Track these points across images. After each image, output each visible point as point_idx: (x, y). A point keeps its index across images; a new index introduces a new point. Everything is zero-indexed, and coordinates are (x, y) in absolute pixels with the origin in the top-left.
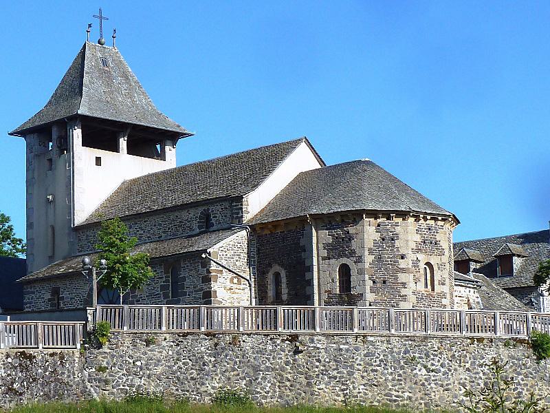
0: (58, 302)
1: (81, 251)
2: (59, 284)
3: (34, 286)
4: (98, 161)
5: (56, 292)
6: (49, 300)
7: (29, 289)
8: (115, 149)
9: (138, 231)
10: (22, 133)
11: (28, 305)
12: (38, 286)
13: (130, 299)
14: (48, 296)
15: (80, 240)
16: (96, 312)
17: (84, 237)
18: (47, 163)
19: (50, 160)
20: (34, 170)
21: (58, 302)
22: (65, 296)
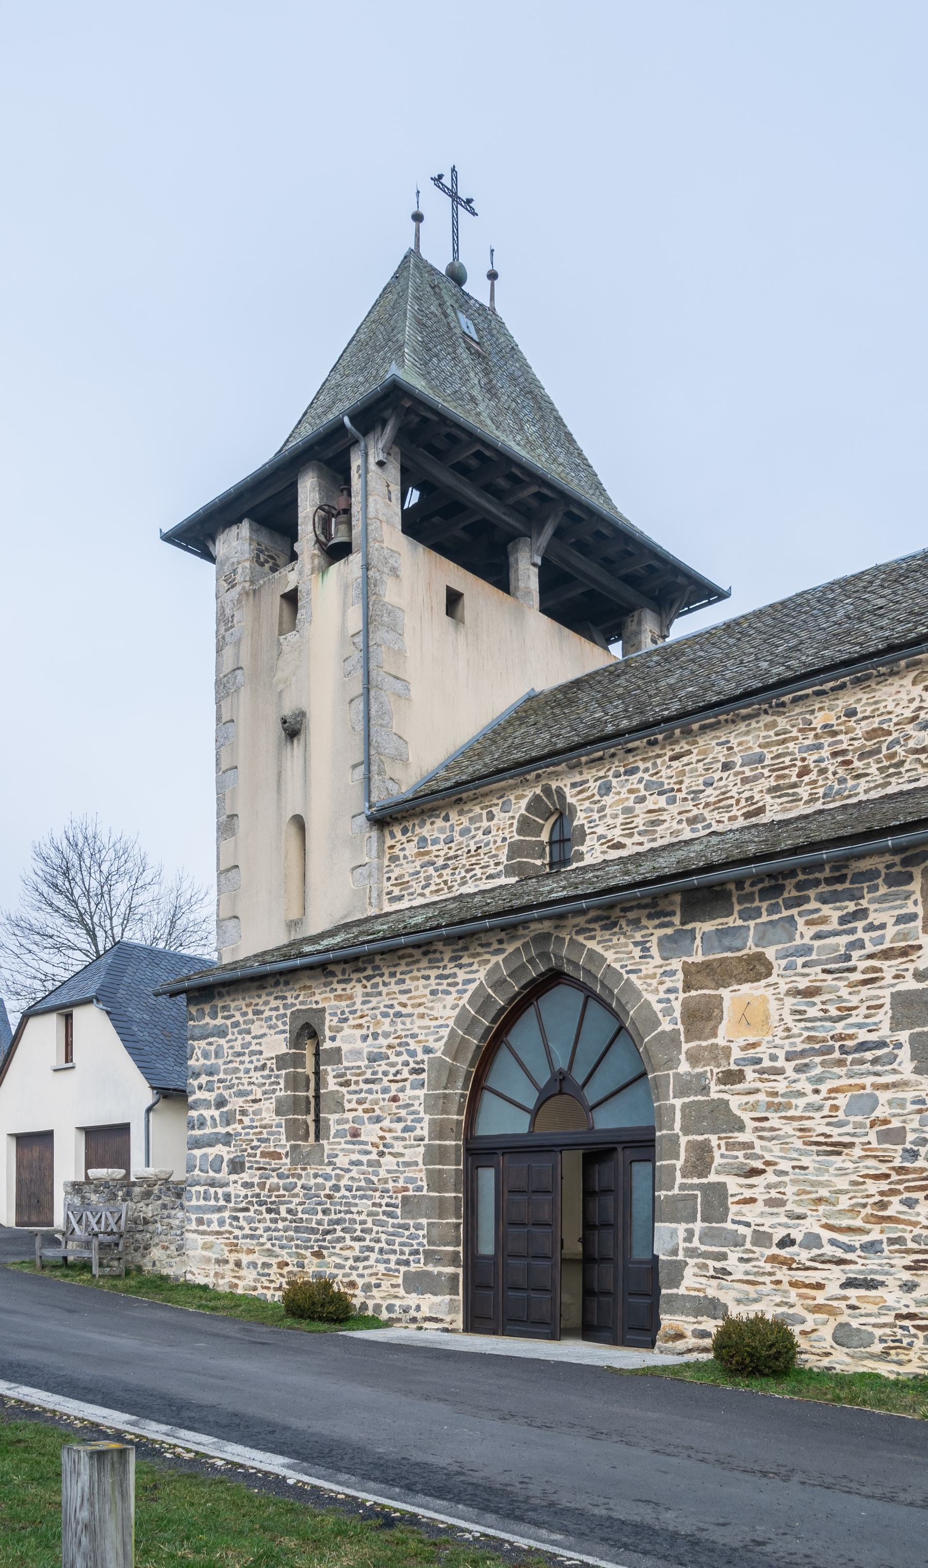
0: (317, 1073)
1: (400, 898)
2: (322, 998)
3: (224, 1008)
4: (453, 599)
5: (307, 1031)
6: (281, 1061)
7: (207, 1020)
8: (500, 577)
9: (642, 800)
10: (197, 535)
11: (203, 1079)
12: (238, 1008)
13: (684, 1067)
14: (277, 1044)
15: (394, 859)
16: (182, 1279)
17: (412, 849)
18: (273, 605)
19: (292, 598)
20: (238, 643)
21: (317, 1073)
22: (345, 1048)
